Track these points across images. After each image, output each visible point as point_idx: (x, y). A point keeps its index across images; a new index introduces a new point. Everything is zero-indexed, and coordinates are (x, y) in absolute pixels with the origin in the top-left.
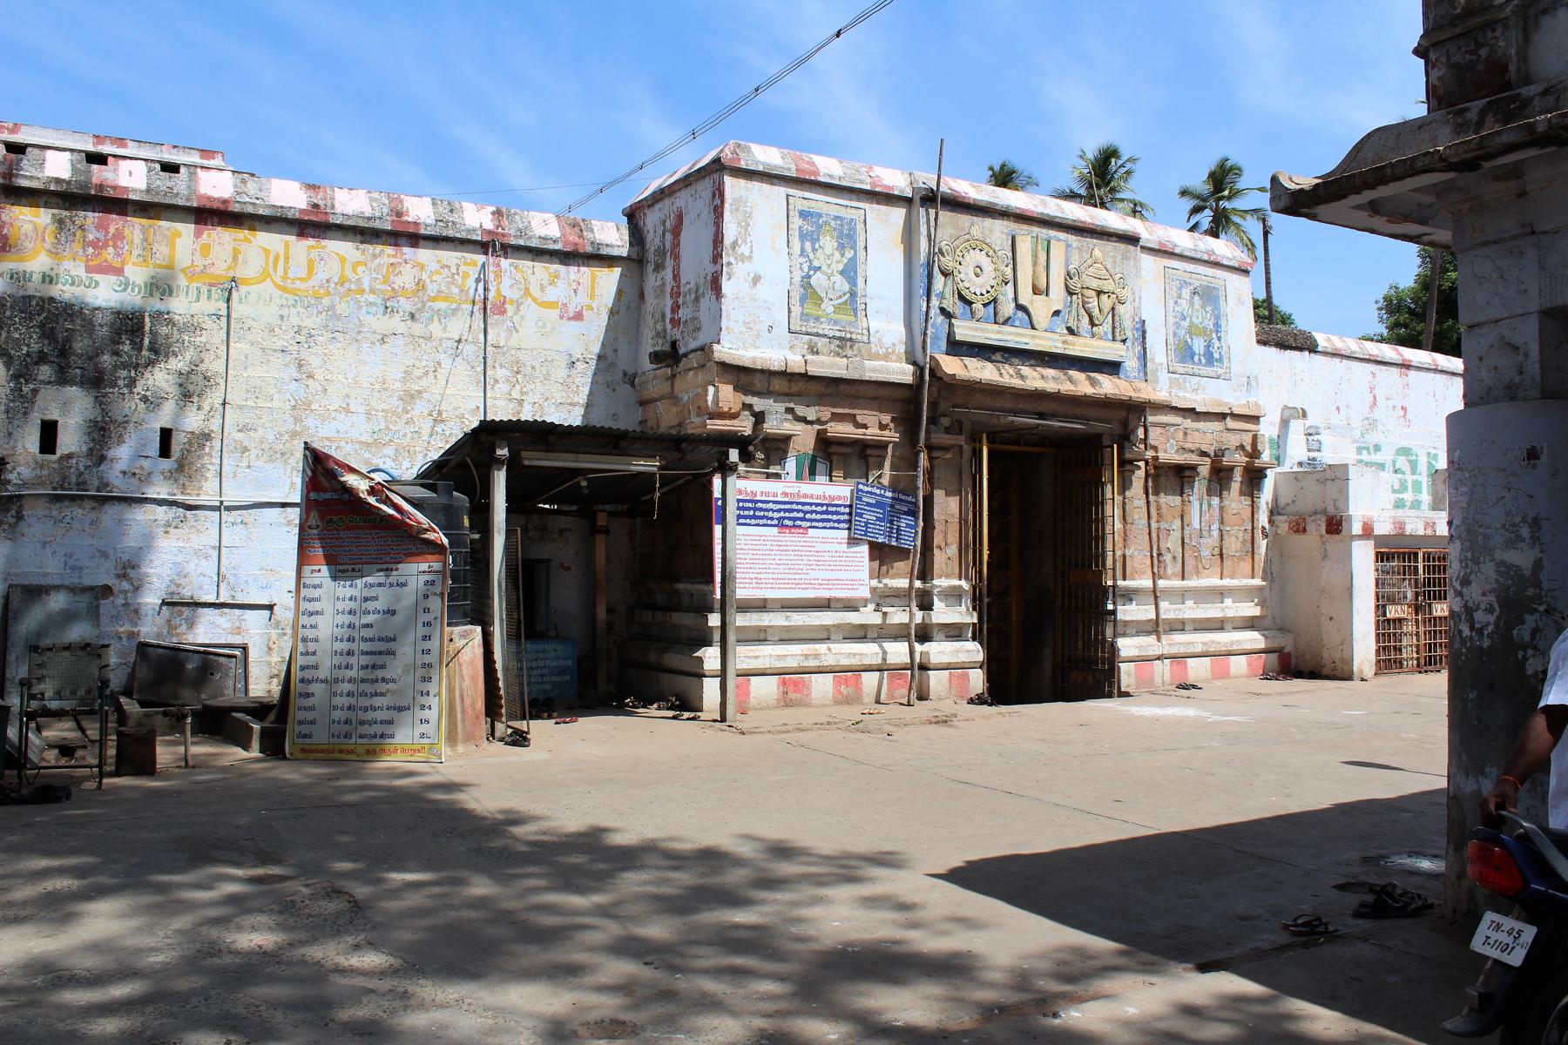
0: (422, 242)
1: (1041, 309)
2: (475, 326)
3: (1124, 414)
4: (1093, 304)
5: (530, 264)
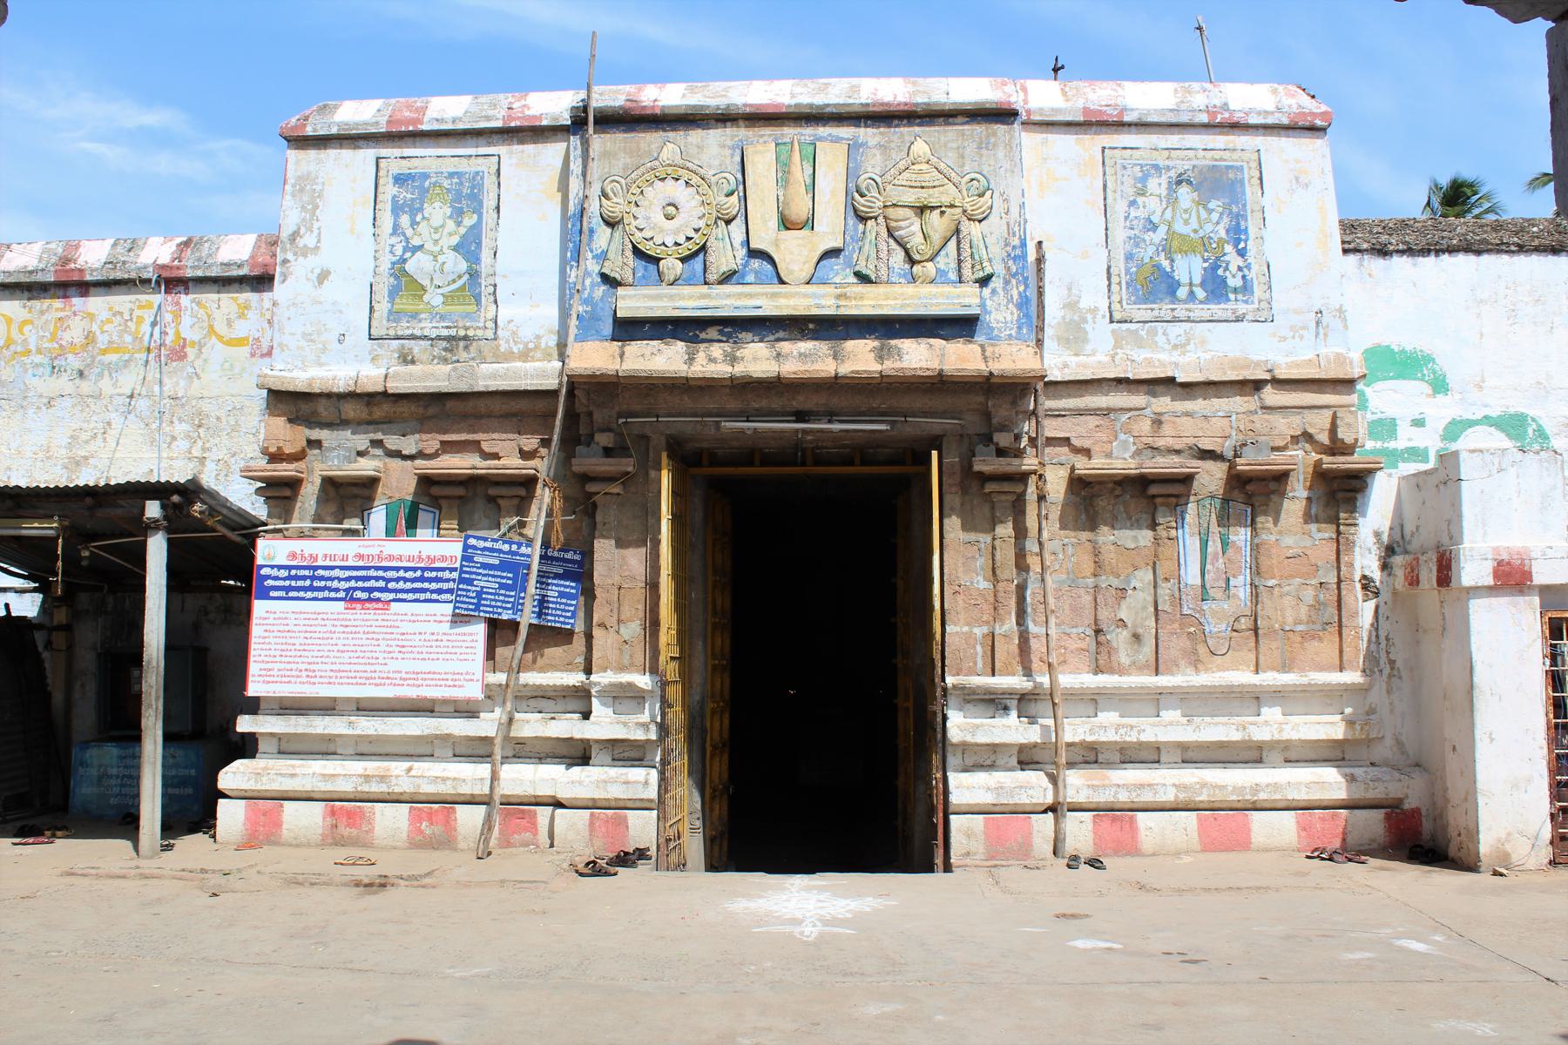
0: (92, 290)
1: (795, 253)
2: (149, 377)
3: (981, 399)
4: (911, 229)
5: (215, 296)
